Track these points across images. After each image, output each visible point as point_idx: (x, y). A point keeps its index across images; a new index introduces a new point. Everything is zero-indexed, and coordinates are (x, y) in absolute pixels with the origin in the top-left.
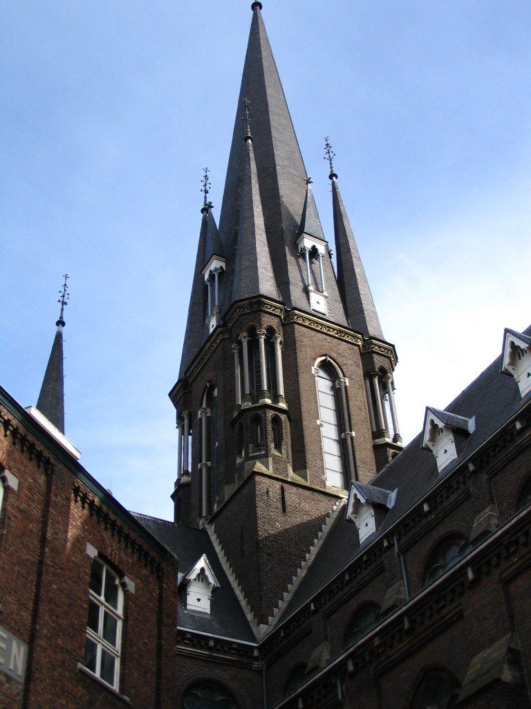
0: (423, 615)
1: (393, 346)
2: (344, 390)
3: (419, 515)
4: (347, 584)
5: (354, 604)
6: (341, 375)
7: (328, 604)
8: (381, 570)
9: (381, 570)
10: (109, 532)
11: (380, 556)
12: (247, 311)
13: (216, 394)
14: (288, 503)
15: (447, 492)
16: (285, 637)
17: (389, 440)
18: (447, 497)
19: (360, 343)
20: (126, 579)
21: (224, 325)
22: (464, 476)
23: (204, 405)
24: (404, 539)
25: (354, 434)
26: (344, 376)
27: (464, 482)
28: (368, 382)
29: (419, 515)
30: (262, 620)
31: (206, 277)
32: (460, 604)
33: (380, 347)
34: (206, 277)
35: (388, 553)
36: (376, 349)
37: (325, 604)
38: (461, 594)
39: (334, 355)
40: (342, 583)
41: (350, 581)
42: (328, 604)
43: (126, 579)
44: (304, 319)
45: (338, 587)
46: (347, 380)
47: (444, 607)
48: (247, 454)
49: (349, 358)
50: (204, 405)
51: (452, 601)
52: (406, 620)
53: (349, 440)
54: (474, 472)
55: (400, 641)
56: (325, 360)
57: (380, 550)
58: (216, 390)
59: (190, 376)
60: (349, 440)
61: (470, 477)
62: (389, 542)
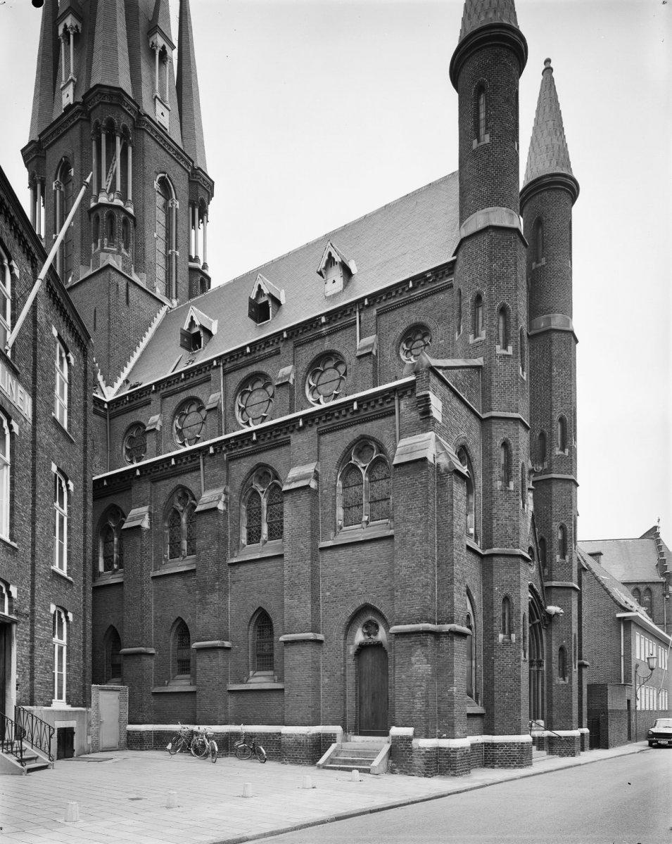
0: (265, 435)
1: (213, 182)
2: (174, 212)
3: (242, 353)
4: (182, 381)
5: (183, 396)
6: (174, 197)
7: (165, 390)
8: (208, 380)
9: (208, 380)
10: (62, 319)
11: (209, 370)
12: (107, 100)
13: (72, 174)
14: (131, 298)
15: (265, 345)
16: (130, 401)
17: (200, 267)
18: (264, 349)
19: (190, 171)
20: (70, 355)
21: (84, 104)
22: (279, 339)
23: (58, 179)
24: (228, 366)
25: (178, 253)
26: (176, 198)
27: (277, 343)
28: (191, 208)
29: (242, 353)
30: (109, 384)
31: (61, 32)
32: (290, 437)
33: (204, 180)
34: (61, 32)
35: (215, 371)
36: (201, 181)
37: (163, 389)
38: (292, 432)
39: (172, 176)
40: (178, 379)
41: (185, 379)
42: (165, 390)
43: (70, 355)
44: (153, 130)
45: (174, 381)
46: (178, 203)
47: (279, 435)
48: (102, 246)
49: (180, 184)
50: (58, 179)
51: (285, 433)
52: (153, 386)
53: (174, 258)
54: (286, 339)
55: (247, 445)
56: (164, 177)
57: (210, 366)
58: (72, 169)
59: (45, 141)
60: (174, 258)
61: (282, 341)
62: (217, 363)
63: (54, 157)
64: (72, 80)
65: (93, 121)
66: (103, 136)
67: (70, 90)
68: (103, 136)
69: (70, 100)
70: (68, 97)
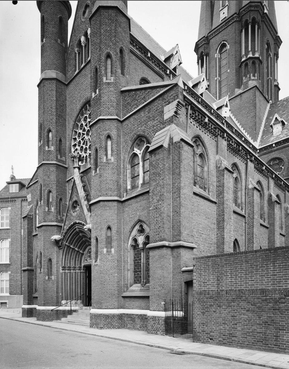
63: (215, 42)
64: (227, 5)
65: (244, 20)
66: (250, 26)
67: (225, 10)
68: (250, 26)
69: (226, 15)
70: (224, 14)
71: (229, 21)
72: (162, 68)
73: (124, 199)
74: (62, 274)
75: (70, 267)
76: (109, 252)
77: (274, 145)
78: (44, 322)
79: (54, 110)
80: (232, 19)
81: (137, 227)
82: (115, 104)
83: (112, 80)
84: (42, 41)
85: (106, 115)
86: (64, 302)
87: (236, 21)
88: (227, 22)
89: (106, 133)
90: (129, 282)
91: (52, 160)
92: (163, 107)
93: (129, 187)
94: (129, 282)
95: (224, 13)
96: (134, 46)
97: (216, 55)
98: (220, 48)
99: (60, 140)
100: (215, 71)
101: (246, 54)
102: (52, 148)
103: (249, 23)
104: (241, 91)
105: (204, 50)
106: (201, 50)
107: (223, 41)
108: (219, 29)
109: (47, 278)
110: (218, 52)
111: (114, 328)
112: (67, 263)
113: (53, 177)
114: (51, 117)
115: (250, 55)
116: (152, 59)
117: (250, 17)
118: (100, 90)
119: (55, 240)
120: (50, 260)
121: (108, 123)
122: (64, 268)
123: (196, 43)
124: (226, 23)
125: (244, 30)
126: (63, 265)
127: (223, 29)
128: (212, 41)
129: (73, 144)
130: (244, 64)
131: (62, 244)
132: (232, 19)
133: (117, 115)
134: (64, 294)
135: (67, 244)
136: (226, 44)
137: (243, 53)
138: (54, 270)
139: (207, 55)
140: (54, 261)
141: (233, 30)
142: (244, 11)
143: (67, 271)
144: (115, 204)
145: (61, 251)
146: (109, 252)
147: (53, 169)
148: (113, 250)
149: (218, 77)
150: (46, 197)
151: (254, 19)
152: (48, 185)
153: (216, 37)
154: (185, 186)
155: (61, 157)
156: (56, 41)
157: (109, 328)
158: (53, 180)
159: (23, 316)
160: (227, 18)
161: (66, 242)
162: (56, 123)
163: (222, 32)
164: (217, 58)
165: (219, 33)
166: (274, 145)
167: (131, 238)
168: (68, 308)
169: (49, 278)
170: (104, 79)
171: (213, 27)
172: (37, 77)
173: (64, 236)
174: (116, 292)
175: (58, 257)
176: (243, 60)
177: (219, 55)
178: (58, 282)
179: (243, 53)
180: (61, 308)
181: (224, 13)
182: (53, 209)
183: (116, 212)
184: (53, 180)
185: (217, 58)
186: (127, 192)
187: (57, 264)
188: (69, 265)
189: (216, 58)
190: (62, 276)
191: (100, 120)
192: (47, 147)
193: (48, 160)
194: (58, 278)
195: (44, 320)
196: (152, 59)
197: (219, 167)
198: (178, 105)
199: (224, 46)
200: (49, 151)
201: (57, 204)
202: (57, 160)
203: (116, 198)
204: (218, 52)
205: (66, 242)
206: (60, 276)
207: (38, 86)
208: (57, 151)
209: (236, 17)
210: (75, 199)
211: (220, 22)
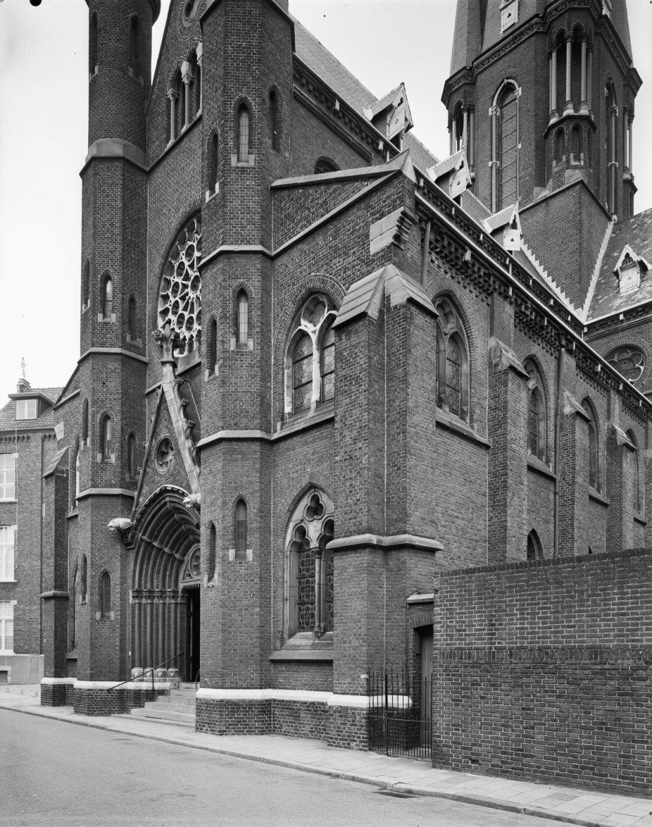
63: (488, 81)
65: (555, 31)
66: (569, 45)
68: (569, 45)
69: (514, 19)
71: (522, 34)
72: (367, 136)
73: (275, 436)
74: (133, 605)
75: (151, 592)
76: (240, 557)
77: (621, 317)
78: (90, 718)
79: (117, 231)
80: (529, 29)
81: (306, 501)
82: (257, 217)
83: (251, 161)
84: (92, 70)
85: (236, 242)
86: (136, 671)
87: (537, 33)
88: (516, 35)
89: (236, 283)
90: (287, 626)
91: (112, 346)
92: (367, 225)
93: (288, 409)
94: (287, 626)
95: (510, 15)
96: (302, 85)
97: (490, 110)
98: (499, 95)
99: (132, 300)
100: (489, 147)
101: (560, 109)
102: (113, 318)
103: (568, 38)
104: (546, 193)
105: (465, 98)
106: (457, 98)
107: (507, 78)
108: (498, 51)
109: (98, 615)
110: (494, 104)
111: (250, 732)
112: (146, 582)
113: (114, 384)
114: (111, 247)
115: (569, 111)
116: (344, 116)
117: (569, 23)
118: (223, 185)
119: (118, 529)
120: (106, 575)
121: (242, 260)
122: (138, 594)
123: (447, 82)
124: (516, 38)
125: (554, 55)
126: (136, 587)
127: (507, 51)
128: (482, 77)
129: (160, 309)
130: (554, 131)
131: (133, 537)
132: (529, 29)
133: (262, 243)
134: (137, 653)
135: (145, 538)
136: (513, 85)
137: (553, 106)
138: (115, 598)
139: (471, 109)
140: (115, 577)
141: (532, 53)
142: (556, 10)
143: (144, 601)
144: (256, 447)
145: (132, 555)
146: (240, 557)
147: (114, 365)
148: (250, 553)
149: (494, 161)
150: (97, 429)
151: (577, 29)
152: (102, 401)
153: (492, 69)
154: (417, 407)
155: (133, 338)
156: (125, 72)
157: (239, 732)
158: (113, 389)
159: (43, 703)
160: (517, 26)
161: (144, 534)
162: (123, 259)
163: (506, 58)
164: (494, 117)
165: (498, 60)
166: (621, 317)
167: (291, 525)
168: (145, 686)
169: (102, 616)
170: (234, 159)
171: (486, 47)
172: (80, 153)
173: (139, 521)
174: (257, 650)
175: (124, 568)
176: (553, 121)
177: (499, 109)
178: (123, 626)
179: (553, 106)
180: (130, 686)
181: (510, 15)
182: (113, 458)
183: (258, 466)
184: (113, 389)
185: (494, 117)
186: (282, 419)
187: (122, 584)
188: (149, 586)
189: (492, 116)
190: (133, 613)
191: (222, 253)
192: (100, 316)
193: (103, 345)
194: (123, 614)
195: (91, 713)
196: (344, 116)
197: (496, 365)
198: (401, 220)
199: (509, 89)
200: (106, 324)
201: (122, 446)
202: (124, 345)
203: (258, 434)
204: (494, 104)
205: (144, 534)
206: (129, 611)
207: (83, 174)
208: (123, 324)
209: (536, 23)
210: (163, 434)
211: (501, 35)
